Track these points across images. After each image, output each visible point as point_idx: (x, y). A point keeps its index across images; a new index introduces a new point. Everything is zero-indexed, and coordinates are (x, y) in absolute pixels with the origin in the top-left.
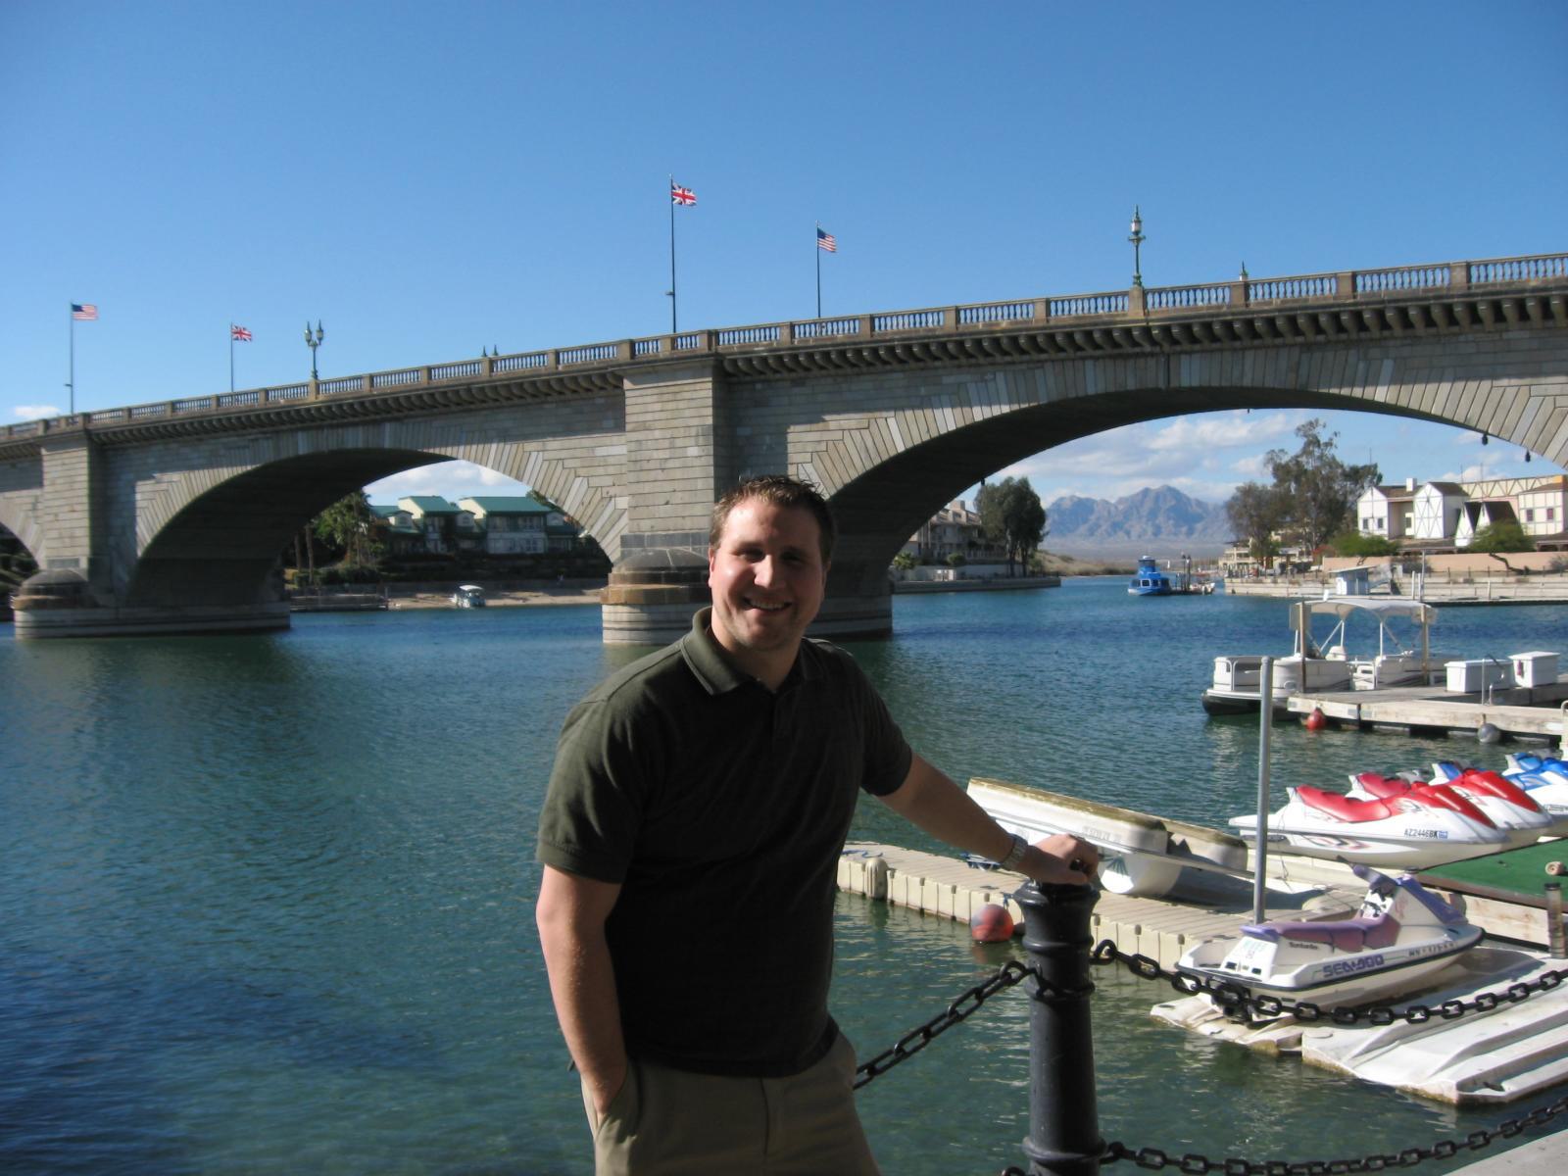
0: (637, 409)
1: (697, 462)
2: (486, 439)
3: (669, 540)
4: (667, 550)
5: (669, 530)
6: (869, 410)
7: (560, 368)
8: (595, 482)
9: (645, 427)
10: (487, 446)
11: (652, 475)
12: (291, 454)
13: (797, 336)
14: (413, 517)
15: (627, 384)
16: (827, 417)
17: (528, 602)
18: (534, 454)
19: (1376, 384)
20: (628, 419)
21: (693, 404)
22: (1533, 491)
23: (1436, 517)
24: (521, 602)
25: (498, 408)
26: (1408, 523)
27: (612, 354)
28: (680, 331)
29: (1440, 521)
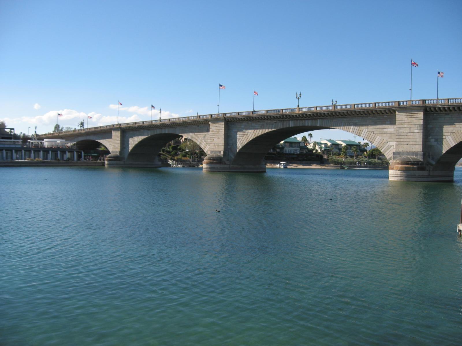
0: (399, 119)
1: (417, 134)
2: (349, 125)
3: (408, 154)
4: (409, 156)
5: (408, 151)
7: (376, 108)
8: (383, 138)
9: (402, 124)
10: (350, 127)
11: (403, 137)
12: (288, 126)
13: (376, 106)
14: (328, 145)
15: (397, 113)
16: (456, 124)
17: (297, 167)
18: (364, 130)
20: (396, 122)
21: (417, 119)
24: (296, 167)
25: (354, 117)
27: (392, 104)
28: (219, 113)
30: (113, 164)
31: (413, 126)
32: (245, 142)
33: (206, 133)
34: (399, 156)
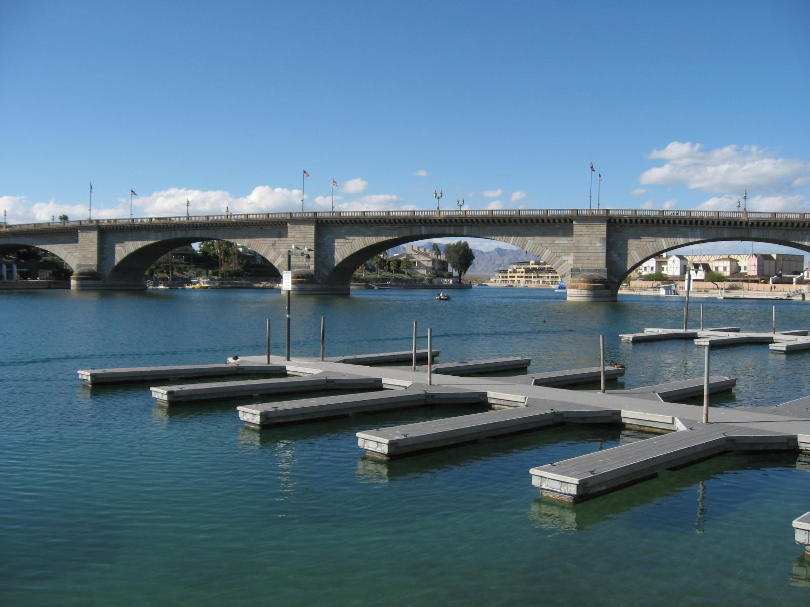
0: (578, 230)
2: (510, 235)
8: (554, 251)
9: (581, 236)
11: (583, 251)
15: (574, 222)
19: (805, 241)
20: (574, 233)
21: (599, 230)
22: (719, 260)
23: (677, 268)
26: (663, 269)
29: (679, 269)
30: (88, 286)
31: (594, 238)
32: (125, 255)
33: (277, 239)
34: (578, 273)
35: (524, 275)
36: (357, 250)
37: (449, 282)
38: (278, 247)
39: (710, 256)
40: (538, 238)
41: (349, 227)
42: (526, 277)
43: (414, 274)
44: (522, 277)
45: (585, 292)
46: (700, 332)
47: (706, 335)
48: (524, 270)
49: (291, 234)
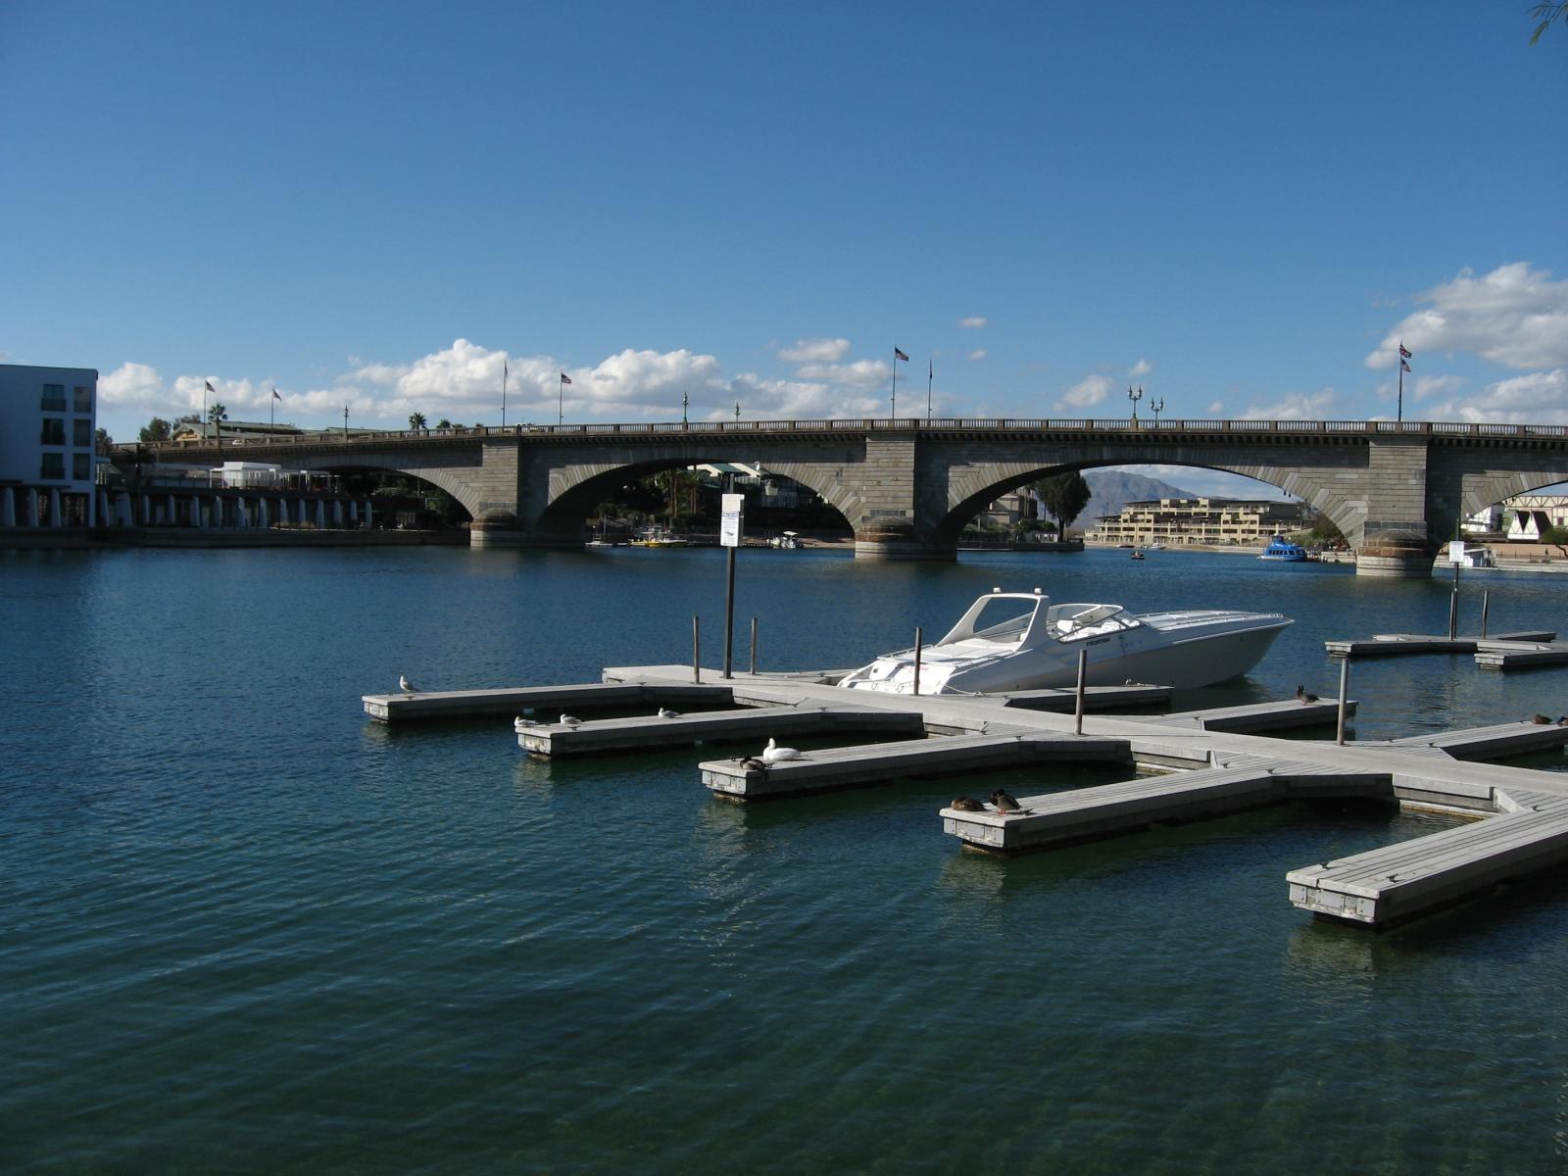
0: (1377, 457)
6: (1507, 470)
8: (1334, 491)
9: (1382, 467)
11: (1385, 492)
14: (711, 475)
15: (1371, 444)
20: (1370, 462)
31: (1406, 472)
33: (843, 465)
35: (1256, 527)
36: (988, 485)
37: (1051, 539)
38: (846, 478)
39: (1545, 499)
40: (1305, 470)
41: (974, 445)
42: (1156, 530)
43: (991, 524)
44: (1149, 529)
45: (1391, 561)
46: (1481, 644)
47: (1494, 650)
48: (1151, 517)
49: (873, 456)
